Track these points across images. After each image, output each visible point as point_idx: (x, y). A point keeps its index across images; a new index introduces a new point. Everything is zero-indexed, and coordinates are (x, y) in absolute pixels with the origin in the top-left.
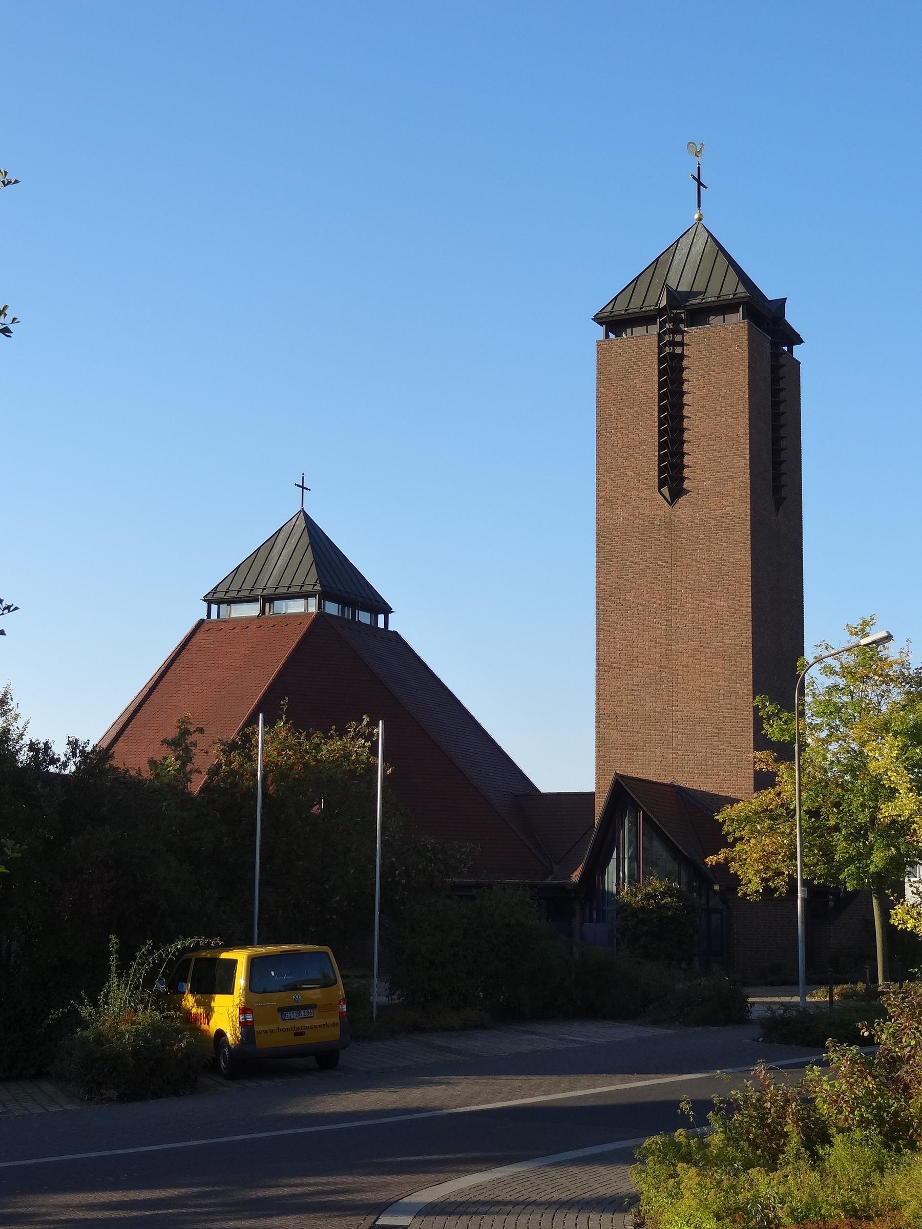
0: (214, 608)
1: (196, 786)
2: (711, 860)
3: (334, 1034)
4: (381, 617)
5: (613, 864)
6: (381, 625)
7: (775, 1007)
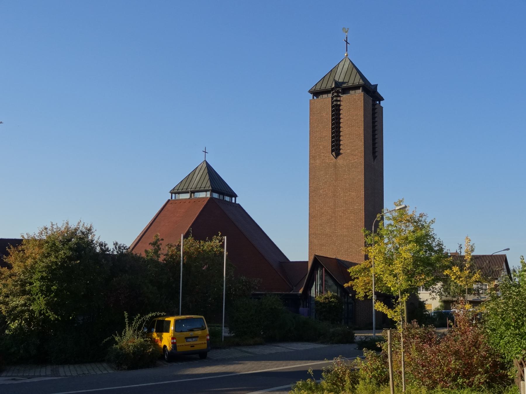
0: (174, 195)
1: (161, 259)
2: (346, 285)
3: (205, 346)
4: (233, 199)
5: (314, 286)
6: (233, 201)
7: (363, 337)
